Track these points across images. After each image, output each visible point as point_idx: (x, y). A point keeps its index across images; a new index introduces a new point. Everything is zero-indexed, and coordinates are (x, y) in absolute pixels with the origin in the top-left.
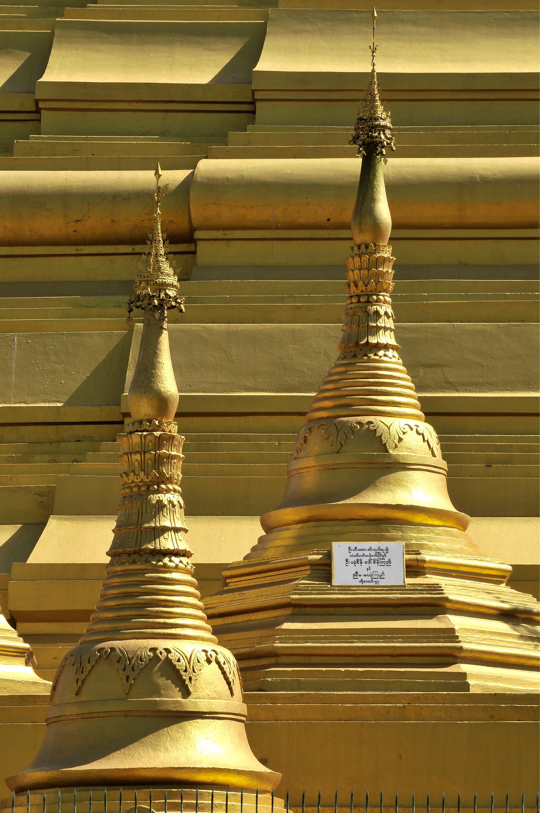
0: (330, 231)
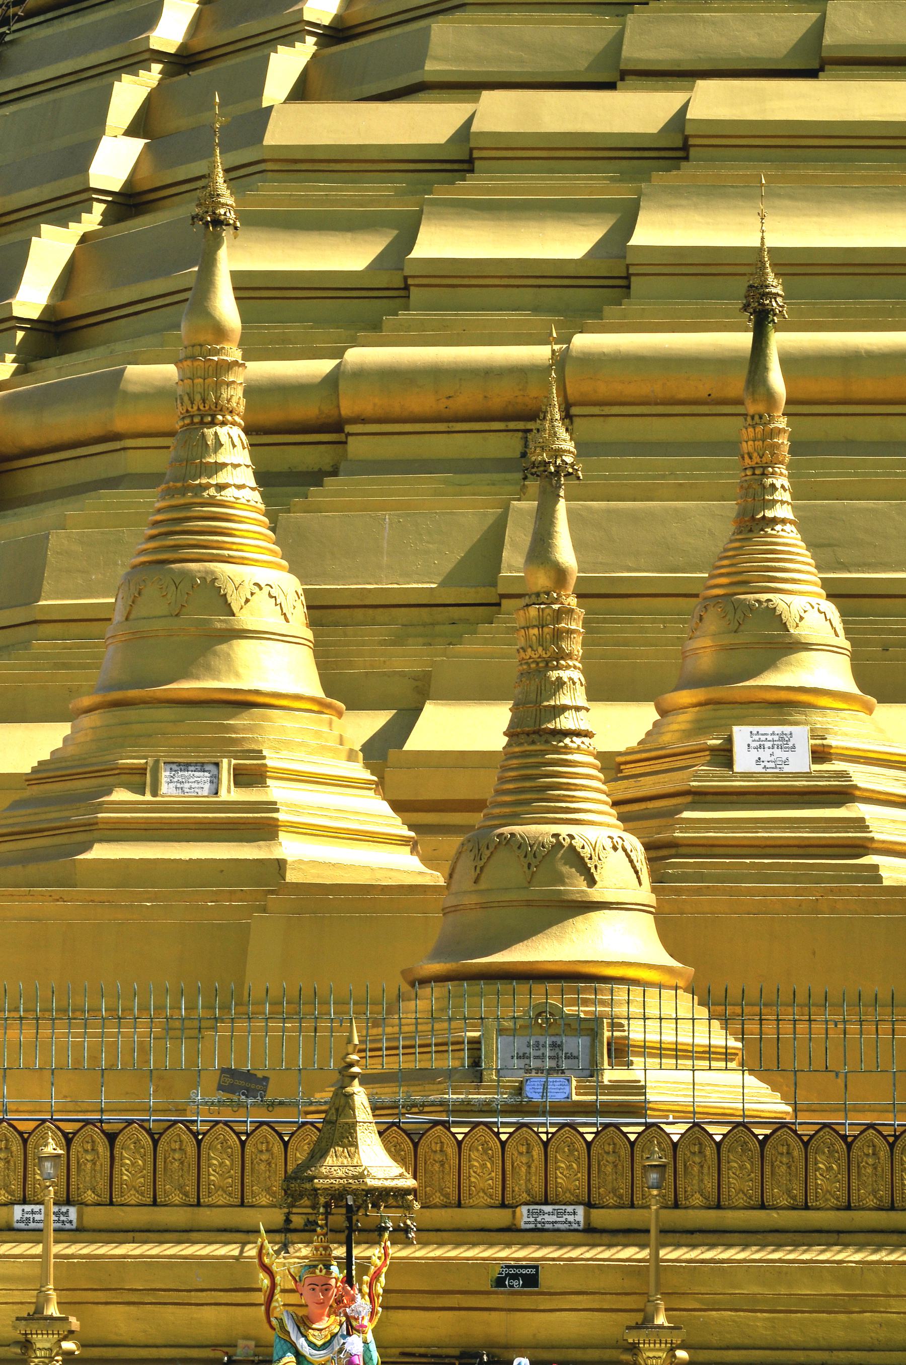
0: (711, 407)
